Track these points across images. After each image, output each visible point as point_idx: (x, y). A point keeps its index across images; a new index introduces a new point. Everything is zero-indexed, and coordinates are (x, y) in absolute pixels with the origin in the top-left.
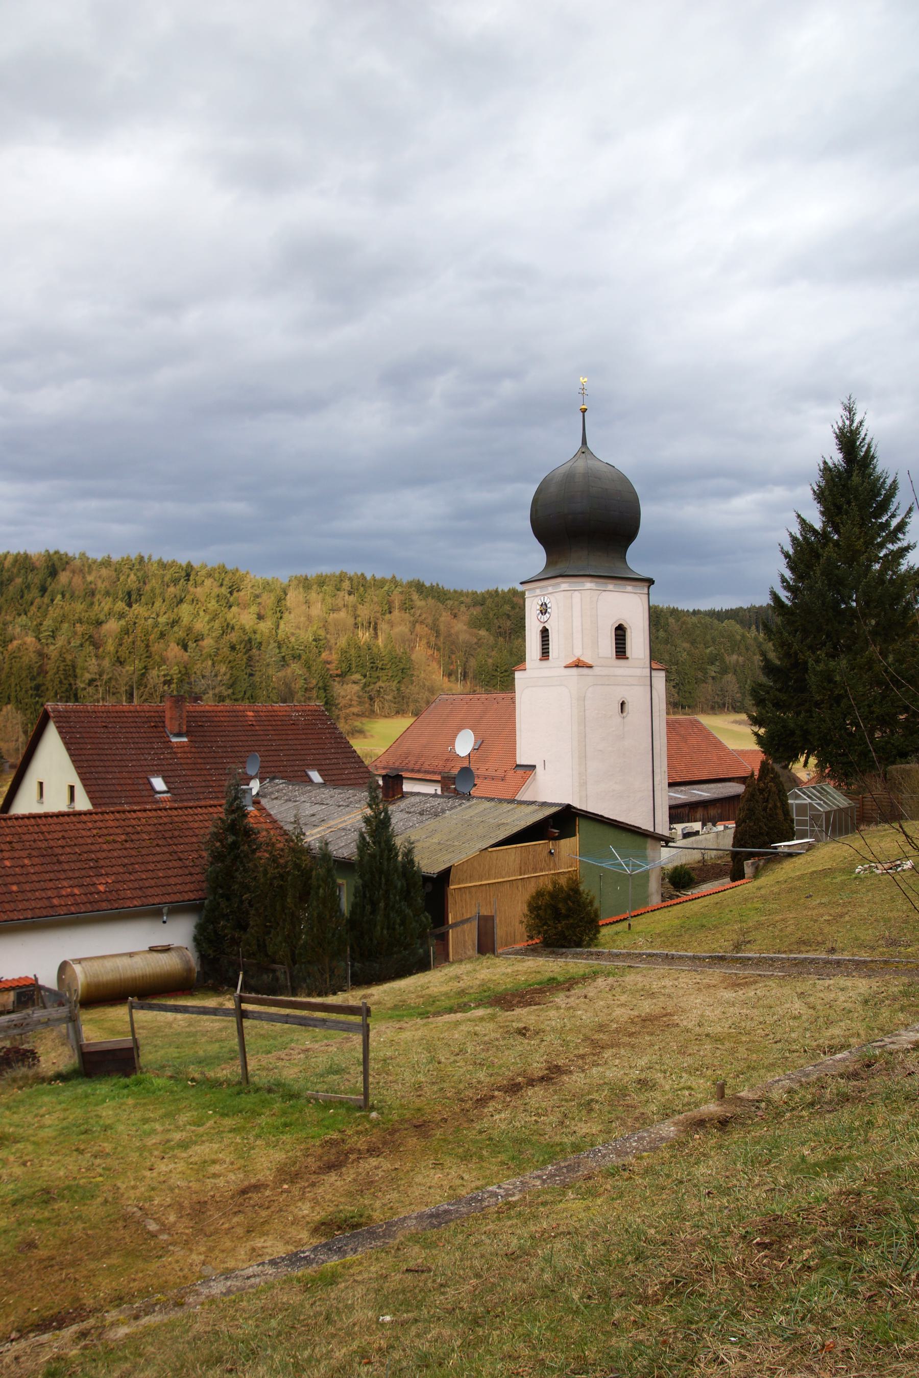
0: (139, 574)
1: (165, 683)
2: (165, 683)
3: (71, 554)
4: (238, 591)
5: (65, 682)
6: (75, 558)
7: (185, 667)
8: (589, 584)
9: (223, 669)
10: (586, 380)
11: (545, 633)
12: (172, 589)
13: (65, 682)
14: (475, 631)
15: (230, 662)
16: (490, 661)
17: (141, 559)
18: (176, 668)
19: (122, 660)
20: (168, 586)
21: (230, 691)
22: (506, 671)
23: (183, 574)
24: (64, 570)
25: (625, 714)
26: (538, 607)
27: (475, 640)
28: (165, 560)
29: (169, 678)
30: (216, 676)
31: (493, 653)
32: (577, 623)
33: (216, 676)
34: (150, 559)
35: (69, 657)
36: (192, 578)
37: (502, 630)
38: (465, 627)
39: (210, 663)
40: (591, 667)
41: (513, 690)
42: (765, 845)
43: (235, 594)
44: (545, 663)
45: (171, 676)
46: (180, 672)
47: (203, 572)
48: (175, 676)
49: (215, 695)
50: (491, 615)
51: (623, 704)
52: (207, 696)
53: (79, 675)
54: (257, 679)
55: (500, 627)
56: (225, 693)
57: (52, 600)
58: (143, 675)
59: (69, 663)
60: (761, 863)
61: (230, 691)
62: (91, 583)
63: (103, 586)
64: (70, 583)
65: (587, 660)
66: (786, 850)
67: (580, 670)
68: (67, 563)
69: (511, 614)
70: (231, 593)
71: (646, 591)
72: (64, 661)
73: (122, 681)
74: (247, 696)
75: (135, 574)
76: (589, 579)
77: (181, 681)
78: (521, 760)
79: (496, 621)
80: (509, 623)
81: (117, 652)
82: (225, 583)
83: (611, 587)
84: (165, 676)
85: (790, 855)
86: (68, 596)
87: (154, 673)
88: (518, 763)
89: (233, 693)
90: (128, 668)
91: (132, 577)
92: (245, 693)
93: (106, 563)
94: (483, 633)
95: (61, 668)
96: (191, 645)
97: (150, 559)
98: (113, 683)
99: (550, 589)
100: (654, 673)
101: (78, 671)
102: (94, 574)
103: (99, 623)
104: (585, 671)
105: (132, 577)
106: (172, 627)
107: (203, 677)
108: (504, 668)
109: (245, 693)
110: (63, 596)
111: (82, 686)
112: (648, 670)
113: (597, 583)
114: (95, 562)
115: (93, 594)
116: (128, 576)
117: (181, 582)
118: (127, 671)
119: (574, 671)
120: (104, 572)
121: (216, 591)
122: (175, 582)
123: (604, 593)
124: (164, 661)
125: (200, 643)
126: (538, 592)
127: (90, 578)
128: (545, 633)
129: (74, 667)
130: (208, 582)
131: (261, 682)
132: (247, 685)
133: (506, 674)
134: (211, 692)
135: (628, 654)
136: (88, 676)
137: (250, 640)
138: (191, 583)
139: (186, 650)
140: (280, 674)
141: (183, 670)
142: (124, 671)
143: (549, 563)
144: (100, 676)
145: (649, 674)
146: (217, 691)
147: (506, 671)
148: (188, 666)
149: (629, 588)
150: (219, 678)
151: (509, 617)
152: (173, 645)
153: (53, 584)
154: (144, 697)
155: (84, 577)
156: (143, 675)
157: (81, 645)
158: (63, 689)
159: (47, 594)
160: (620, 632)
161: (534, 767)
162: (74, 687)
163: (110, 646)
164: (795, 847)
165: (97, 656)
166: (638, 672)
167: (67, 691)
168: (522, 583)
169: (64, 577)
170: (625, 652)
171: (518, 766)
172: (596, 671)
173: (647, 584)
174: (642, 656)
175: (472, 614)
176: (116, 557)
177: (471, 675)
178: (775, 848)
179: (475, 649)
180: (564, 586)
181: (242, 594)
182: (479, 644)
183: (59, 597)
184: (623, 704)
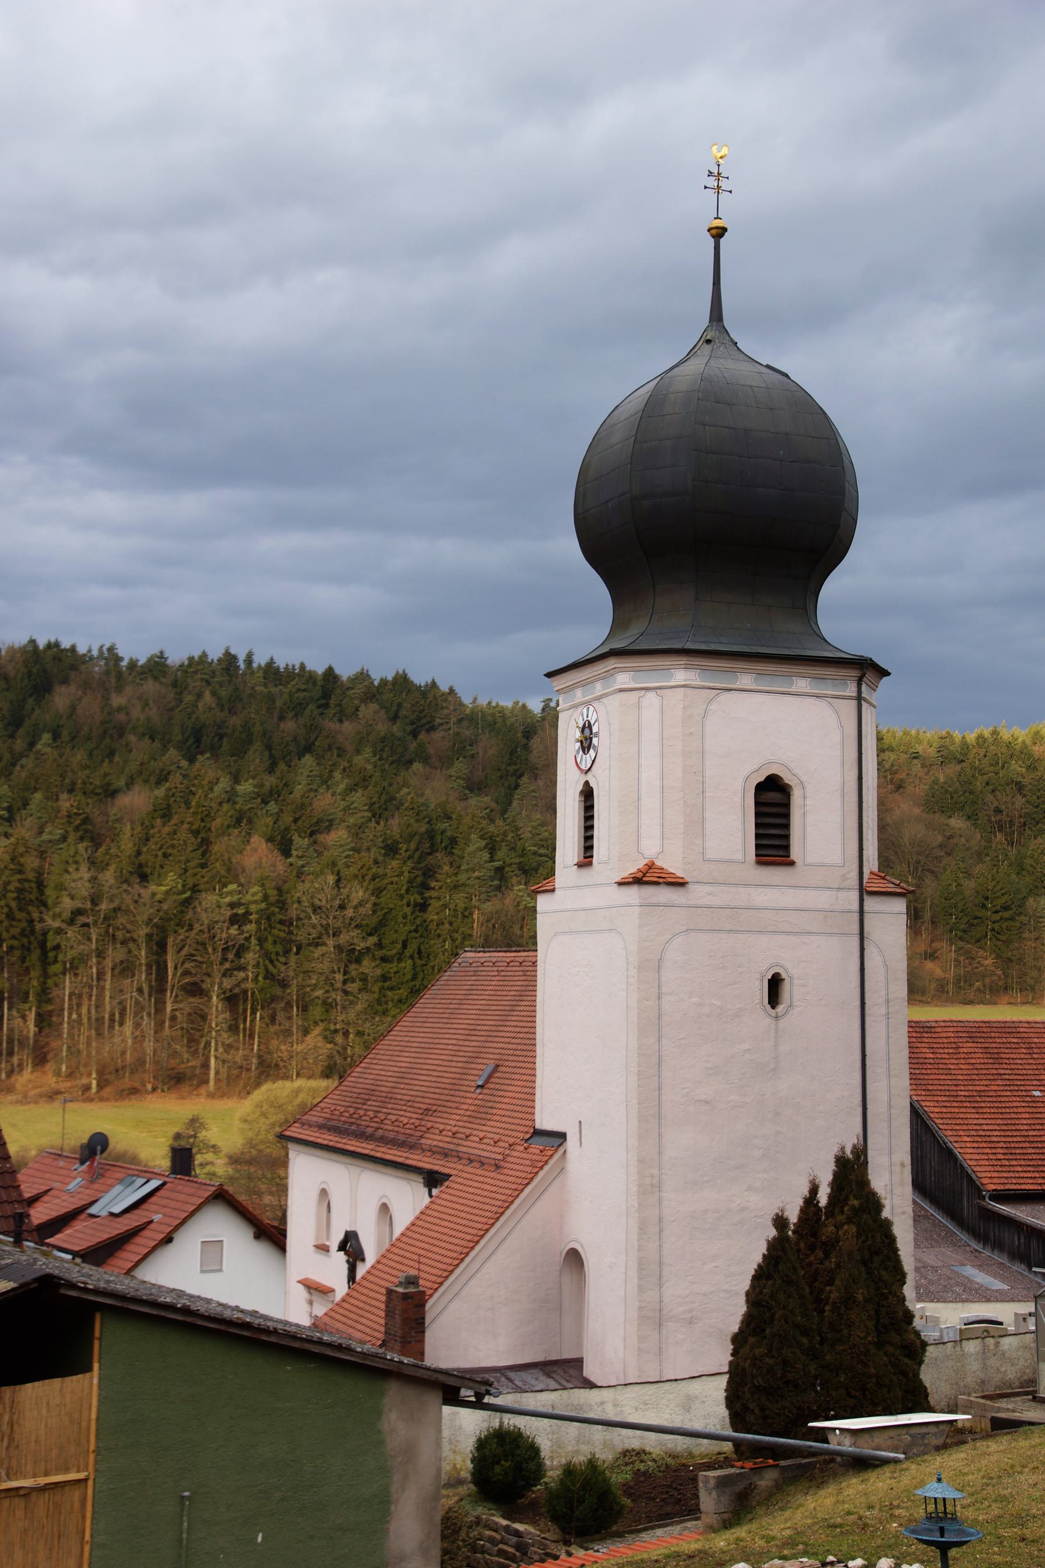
0: (224, 693)
1: (234, 920)
2: (234, 920)
3: (82, 649)
4: (428, 731)
5: (19, 915)
6: (91, 658)
7: (279, 890)
8: (681, 674)
9: (358, 894)
10: (725, 151)
11: (587, 794)
12: (289, 725)
13: (19, 915)
14: (940, 819)
15: (373, 879)
16: (970, 885)
17: (230, 659)
18: (256, 889)
19: (148, 870)
20: (282, 718)
21: (372, 940)
22: (1006, 908)
23: (317, 692)
24: (65, 681)
25: (780, 1009)
26: (578, 734)
27: (940, 839)
28: (281, 663)
29: (241, 911)
30: (342, 907)
31: (979, 868)
32: (650, 773)
33: (342, 907)
34: (249, 660)
35: (31, 862)
36: (333, 702)
37: (1004, 817)
38: (917, 811)
39: (331, 879)
40: (680, 884)
41: (530, 942)
42: (796, 1426)
43: (422, 736)
44: (585, 872)
45: (247, 905)
46: (266, 897)
47: (359, 690)
48: (253, 908)
49: (339, 948)
50: (978, 785)
51: (775, 984)
52: (318, 952)
53: (50, 902)
54: (432, 915)
55: (998, 811)
56: (361, 945)
57: (32, 744)
58: (187, 902)
59: (31, 875)
60: (766, 1481)
61: (372, 940)
62: (120, 709)
63: (142, 717)
64: (73, 708)
65: (673, 864)
66: (847, 1446)
67: (649, 891)
68: (73, 667)
69: (1026, 781)
70: (415, 734)
71: (851, 690)
72: (20, 872)
73: (144, 913)
74: (408, 953)
75: (214, 694)
76: (683, 660)
77: (267, 916)
78: (545, 1121)
79: (990, 797)
80: (1019, 801)
81: (139, 853)
82: (403, 712)
83: (746, 680)
84: (232, 905)
85: (862, 1464)
86: (65, 735)
87: (209, 899)
88: (538, 1126)
89: (379, 945)
90: (153, 888)
91: (207, 697)
92: (405, 945)
93: (157, 667)
94: (957, 823)
95: (11, 887)
96: (300, 842)
97: (249, 660)
98: (121, 920)
99: (599, 688)
100: (870, 903)
101: (49, 892)
102: (128, 690)
103: (111, 793)
104: (663, 894)
105: (207, 697)
106: (265, 802)
107: (316, 909)
108: (1000, 902)
109: (405, 945)
110: (56, 735)
111: (56, 924)
112: (855, 895)
113: (704, 670)
114: (133, 664)
115: (121, 731)
116: (200, 696)
117: (307, 712)
118: (154, 894)
119: (634, 893)
120: (150, 687)
121: (382, 727)
122: (297, 708)
123: (726, 695)
124: (232, 873)
125: (320, 838)
126: (579, 695)
127: (117, 701)
128: (587, 794)
129: (40, 885)
130: (368, 711)
131: (440, 923)
132: (409, 927)
133: (1007, 914)
134: (331, 942)
135: (795, 853)
136: (67, 904)
137: (431, 835)
138: (331, 712)
139: (286, 852)
140: (488, 907)
141: (273, 893)
142: (146, 893)
143: (619, 624)
144: (94, 902)
145: (856, 906)
146: (344, 938)
147: (1006, 908)
148: (286, 887)
149: (802, 684)
150: (349, 913)
151: (1020, 787)
152: (258, 842)
153: (37, 711)
154: (184, 952)
155: (106, 698)
156: (187, 902)
157: (64, 838)
158: (15, 931)
159: (21, 732)
160: (772, 796)
161: (562, 1136)
162: (38, 926)
163: (127, 844)
164: (878, 1439)
165: (92, 862)
166: (823, 899)
167: (22, 933)
168: (550, 675)
169: (61, 698)
170: (787, 848)
171: (538, 1133)
172: (696, 894)
173: (855, 673)
174: (836, 858)
175: (936, 782)
176: (176, 657)
177: (928, 916)
178: (822, 1435)
179: (938, 859)
180: (623, 679)
181: (437, 735)
182: (948, 847)
183: (46, 737)
184: (775, 984)
